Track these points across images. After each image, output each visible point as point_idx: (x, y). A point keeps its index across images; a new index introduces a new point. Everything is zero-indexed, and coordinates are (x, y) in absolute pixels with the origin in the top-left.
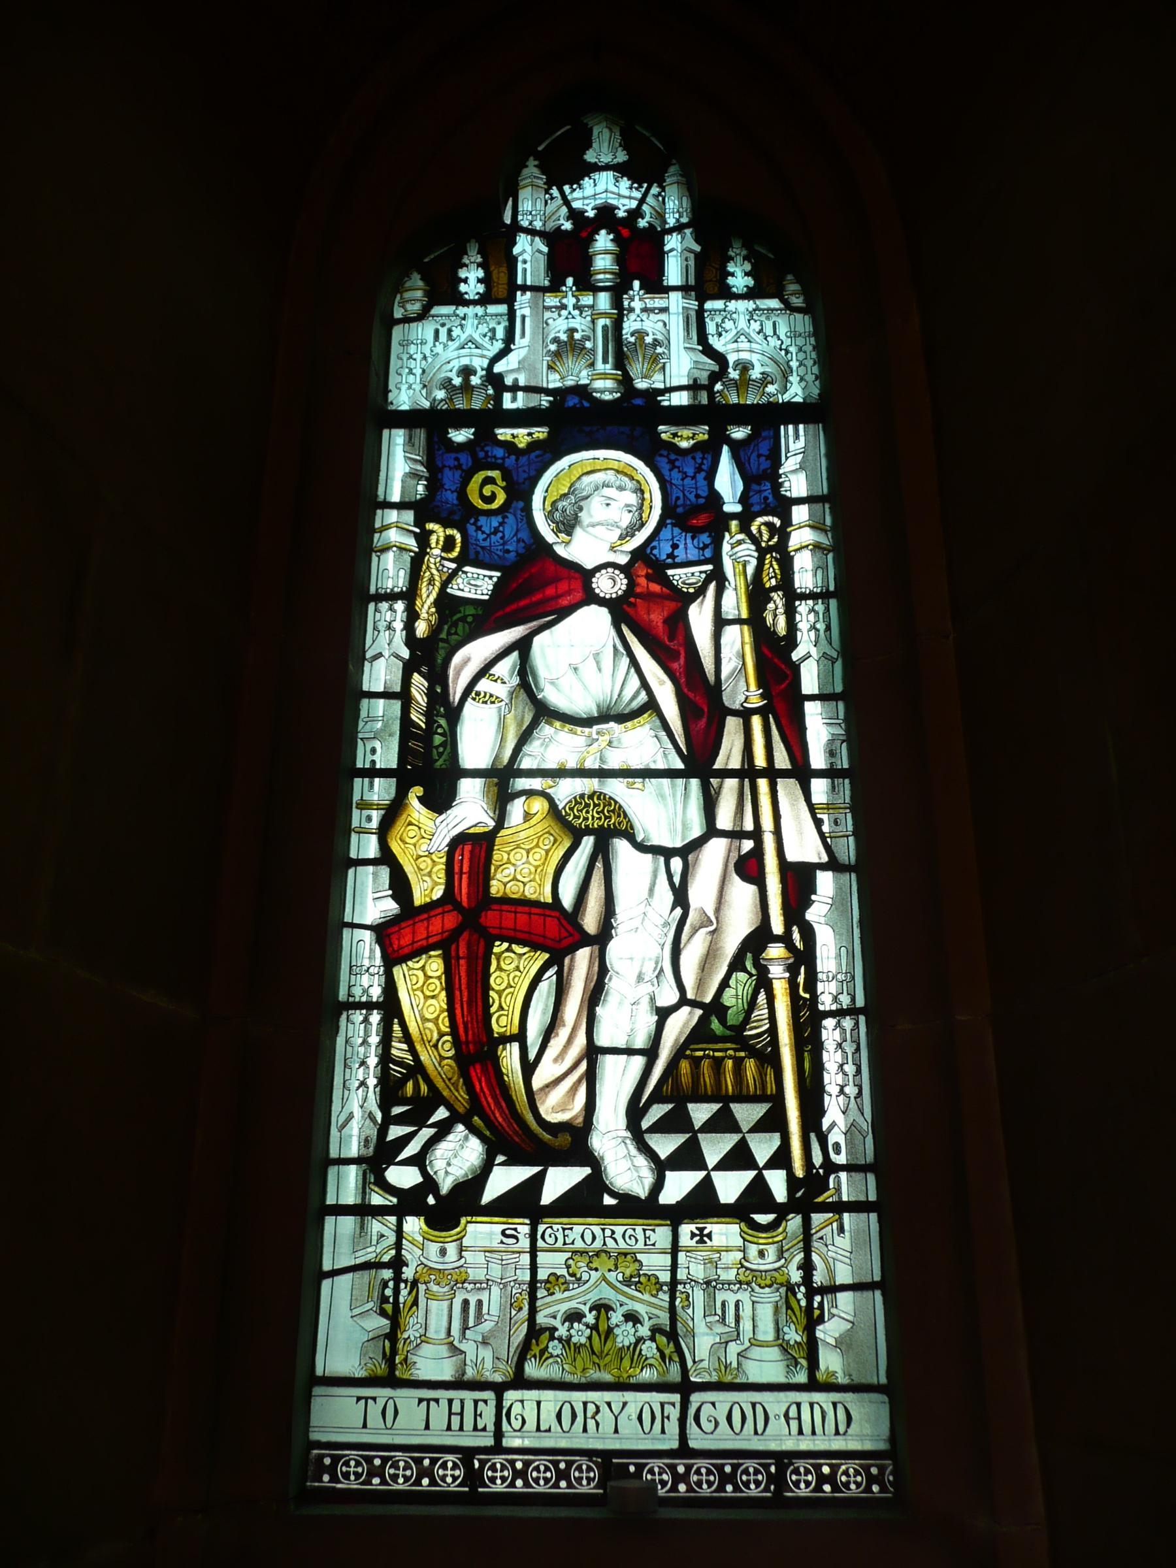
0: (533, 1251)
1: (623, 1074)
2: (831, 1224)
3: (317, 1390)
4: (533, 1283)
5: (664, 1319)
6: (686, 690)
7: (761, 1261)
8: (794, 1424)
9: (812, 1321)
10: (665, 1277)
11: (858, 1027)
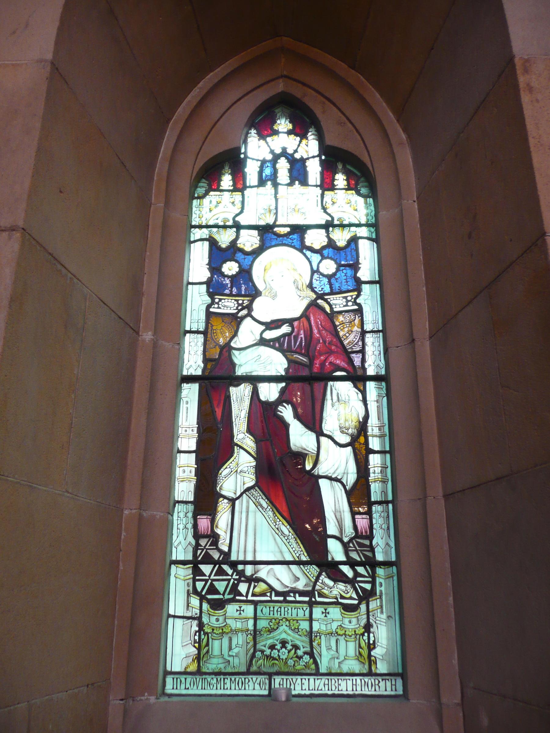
1: (341, 212)
2: (377, 610)
3: (308, 619)
5: (308, 649)
6: (333, 577)
8: (327, 687)
9: (371, 647)
10: (308, 629)
11: (380, 355)
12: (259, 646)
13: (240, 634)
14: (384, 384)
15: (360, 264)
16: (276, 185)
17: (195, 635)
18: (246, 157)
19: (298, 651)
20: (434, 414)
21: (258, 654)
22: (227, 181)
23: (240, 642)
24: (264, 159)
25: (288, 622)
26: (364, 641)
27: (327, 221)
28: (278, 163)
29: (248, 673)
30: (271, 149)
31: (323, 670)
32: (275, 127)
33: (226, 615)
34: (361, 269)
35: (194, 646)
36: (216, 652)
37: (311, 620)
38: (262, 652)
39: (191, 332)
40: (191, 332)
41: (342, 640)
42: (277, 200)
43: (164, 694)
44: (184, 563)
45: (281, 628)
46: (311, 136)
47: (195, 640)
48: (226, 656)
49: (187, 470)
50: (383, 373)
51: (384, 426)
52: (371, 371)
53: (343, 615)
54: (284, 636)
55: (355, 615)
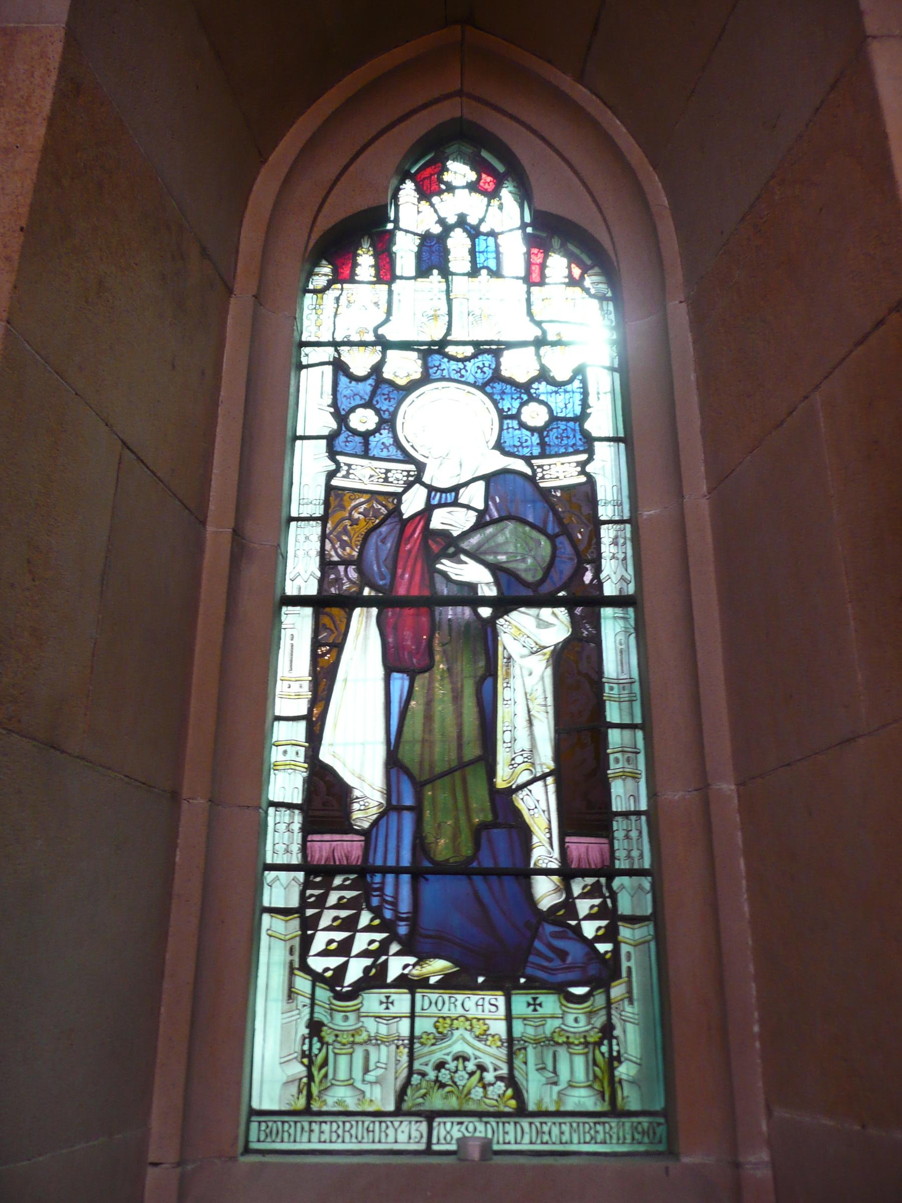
0: (412, 1016)
4: (412, 1037)
5: (504, 1071)
7: (576, 1025)
9: (614, 1060)
10: (504, 1036)
12: (417, 1065)
13: (383, 1047)
14: (631, 611)
15: (590, 407)
16: (446, 273)
17: (303, 1044)
18: (397, 227)
19: (485, 1074)
20: (707, 513)
21: (416, 1079)
22: (365, 262)
23: (384, 1059)
24: (428, 232)
25: (468, 1023)
26: (603, 1054)
27: (537, 337)
28: (450, 237)
29: (398, 1112)
30: (439, 216)
31: (532, 1107)
32: (446, 177)
33: (362, 1010)
34: (591, 416)
35: (302, 1063)
36: (342, 1075)
37: (509, 1018)
38: (423, 1074)
39: (298, 519)
40: (298, 519)
41: (562, 1052)
42: (449, 301)
43: (247, 1151)
44: (284, 912)
45: (457, 1034)
46: (507, 194)
47: (303, 1052)
48: (359, 1084)
49: (291, 750)
50: (631, 589)
51: (639, 753)
52: (609, 590)
53: (564, 1008)
54: (459, 1047)
55: (583, 1009)
